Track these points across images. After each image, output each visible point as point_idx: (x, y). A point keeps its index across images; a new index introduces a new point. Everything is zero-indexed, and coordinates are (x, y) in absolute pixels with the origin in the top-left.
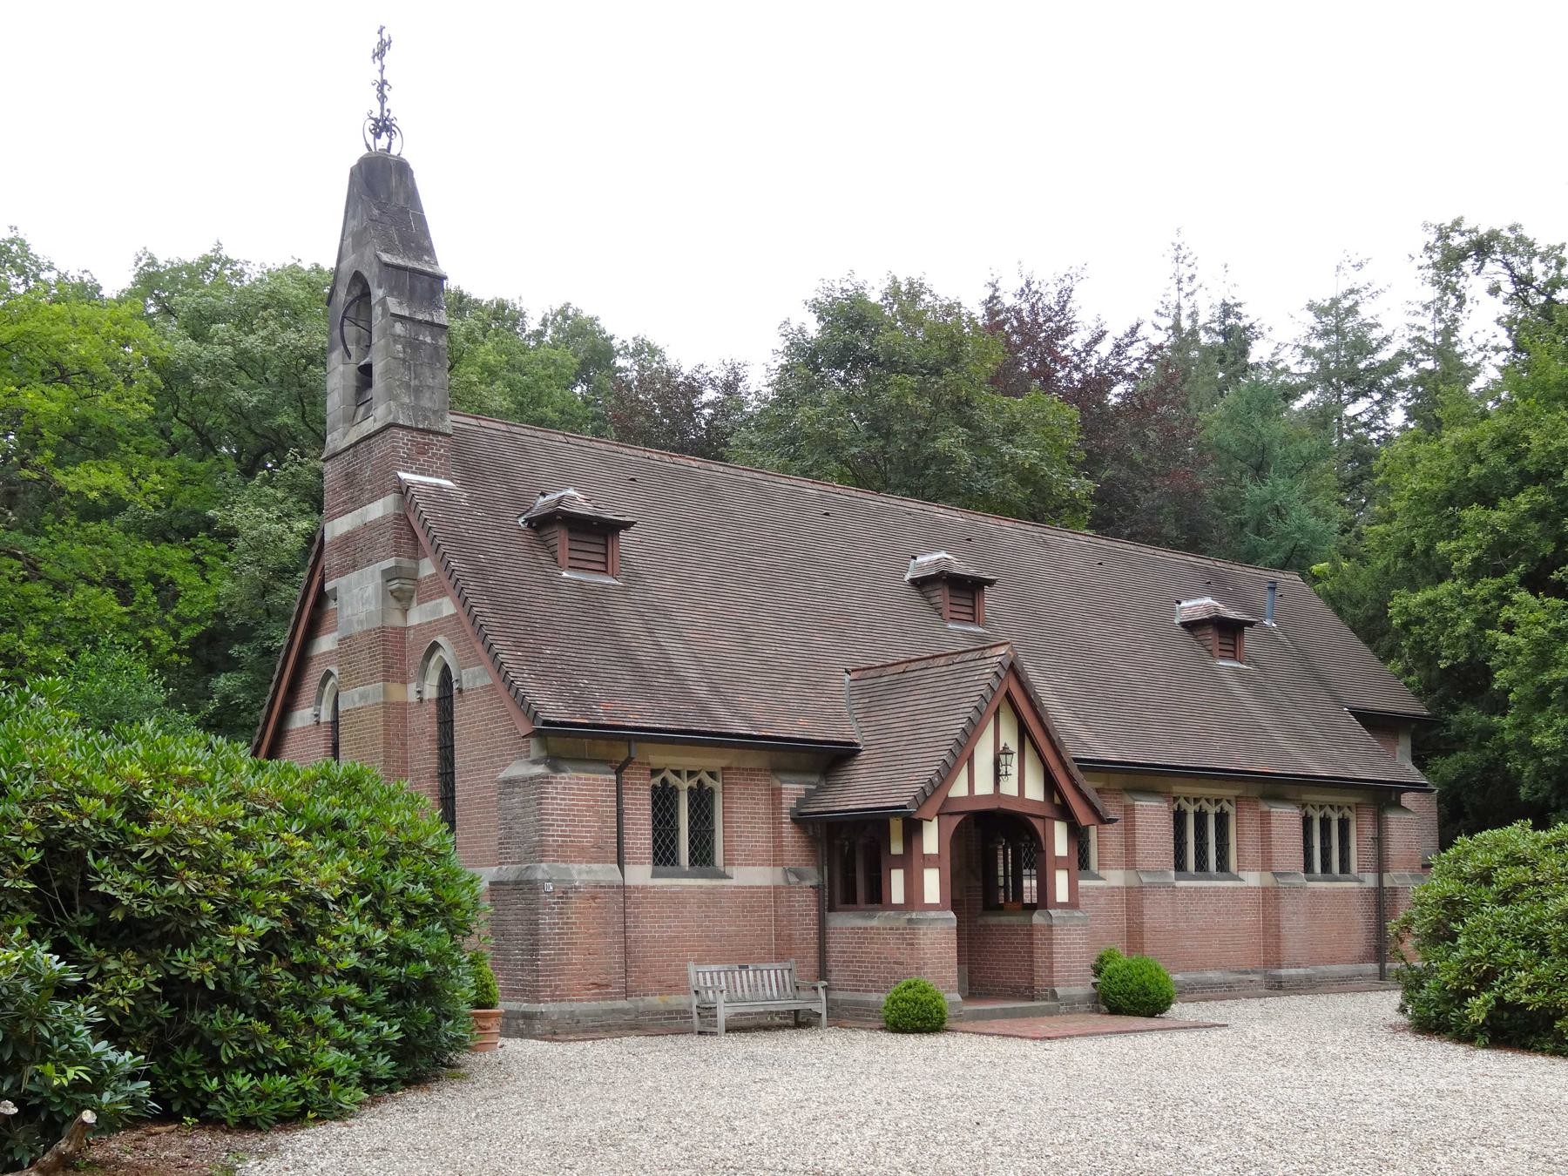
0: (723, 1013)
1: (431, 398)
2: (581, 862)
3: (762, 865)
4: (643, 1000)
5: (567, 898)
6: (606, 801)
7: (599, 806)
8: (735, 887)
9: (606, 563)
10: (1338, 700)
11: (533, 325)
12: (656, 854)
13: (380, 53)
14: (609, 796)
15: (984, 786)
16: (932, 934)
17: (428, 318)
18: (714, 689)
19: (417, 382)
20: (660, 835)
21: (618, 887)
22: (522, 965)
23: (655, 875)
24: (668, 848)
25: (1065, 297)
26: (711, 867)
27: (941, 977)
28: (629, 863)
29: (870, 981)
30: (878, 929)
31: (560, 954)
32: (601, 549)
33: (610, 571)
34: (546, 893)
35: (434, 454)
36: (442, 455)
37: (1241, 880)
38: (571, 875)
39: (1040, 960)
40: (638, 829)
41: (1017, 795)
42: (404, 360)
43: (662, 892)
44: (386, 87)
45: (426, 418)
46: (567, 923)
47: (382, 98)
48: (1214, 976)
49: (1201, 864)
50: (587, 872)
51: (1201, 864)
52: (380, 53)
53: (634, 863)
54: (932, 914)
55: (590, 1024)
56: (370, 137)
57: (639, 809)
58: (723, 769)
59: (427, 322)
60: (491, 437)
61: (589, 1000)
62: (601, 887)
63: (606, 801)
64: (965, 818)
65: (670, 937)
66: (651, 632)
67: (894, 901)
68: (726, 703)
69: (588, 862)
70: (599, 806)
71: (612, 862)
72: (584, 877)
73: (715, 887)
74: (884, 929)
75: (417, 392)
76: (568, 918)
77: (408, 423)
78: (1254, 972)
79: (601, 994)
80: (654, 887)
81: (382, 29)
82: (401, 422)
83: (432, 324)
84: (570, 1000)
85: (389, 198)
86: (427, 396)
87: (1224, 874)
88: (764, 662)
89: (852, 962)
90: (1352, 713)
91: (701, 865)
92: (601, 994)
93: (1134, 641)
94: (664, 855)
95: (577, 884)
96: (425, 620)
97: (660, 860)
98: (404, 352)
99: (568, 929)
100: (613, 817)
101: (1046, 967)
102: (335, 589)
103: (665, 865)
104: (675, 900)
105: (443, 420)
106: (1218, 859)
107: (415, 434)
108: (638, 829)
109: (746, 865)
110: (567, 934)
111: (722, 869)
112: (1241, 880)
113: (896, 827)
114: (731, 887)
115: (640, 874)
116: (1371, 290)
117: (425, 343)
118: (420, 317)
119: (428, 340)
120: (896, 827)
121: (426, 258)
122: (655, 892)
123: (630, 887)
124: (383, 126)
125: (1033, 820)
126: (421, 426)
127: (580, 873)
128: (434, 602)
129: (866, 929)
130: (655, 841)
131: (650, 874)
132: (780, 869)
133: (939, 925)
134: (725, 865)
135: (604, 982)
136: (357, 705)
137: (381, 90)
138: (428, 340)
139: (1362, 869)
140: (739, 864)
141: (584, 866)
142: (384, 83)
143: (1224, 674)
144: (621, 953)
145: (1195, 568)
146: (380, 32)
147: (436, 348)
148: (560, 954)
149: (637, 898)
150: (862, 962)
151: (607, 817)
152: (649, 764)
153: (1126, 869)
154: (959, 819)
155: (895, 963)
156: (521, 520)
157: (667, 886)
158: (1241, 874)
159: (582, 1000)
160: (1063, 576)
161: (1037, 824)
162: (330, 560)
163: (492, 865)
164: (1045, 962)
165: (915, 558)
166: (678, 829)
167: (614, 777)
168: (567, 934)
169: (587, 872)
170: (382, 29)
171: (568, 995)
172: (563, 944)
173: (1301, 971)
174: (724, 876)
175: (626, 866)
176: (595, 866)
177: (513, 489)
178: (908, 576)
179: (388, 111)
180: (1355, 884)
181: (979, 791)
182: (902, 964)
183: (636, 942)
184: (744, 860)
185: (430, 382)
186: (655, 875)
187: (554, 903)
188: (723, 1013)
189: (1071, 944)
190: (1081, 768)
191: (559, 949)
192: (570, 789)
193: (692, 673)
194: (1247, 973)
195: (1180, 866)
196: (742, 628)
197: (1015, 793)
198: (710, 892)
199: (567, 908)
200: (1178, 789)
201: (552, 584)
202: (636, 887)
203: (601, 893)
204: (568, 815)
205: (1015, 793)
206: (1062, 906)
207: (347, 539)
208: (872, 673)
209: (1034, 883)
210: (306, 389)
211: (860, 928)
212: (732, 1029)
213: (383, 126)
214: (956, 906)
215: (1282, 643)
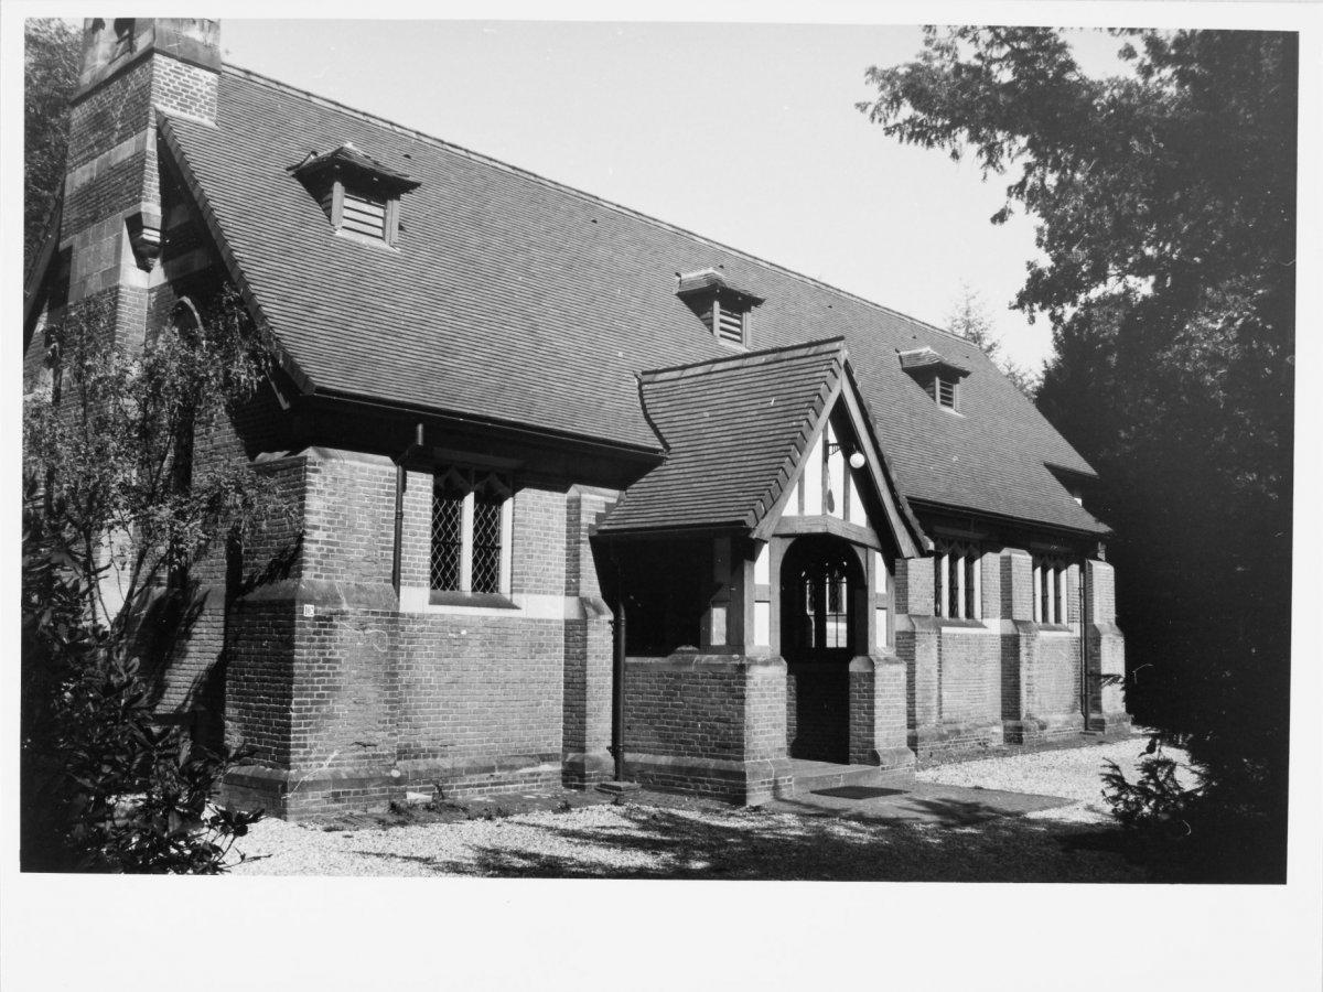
0: (198, 26)
8: (523, 620)
12: (434, 574)
22: (268, 716)
23: (434, 601)
24: (448, 567)
29: (682, 742)
39: (857, 715)
40: (417, 541)
41: (842, 518)
46: (328, 661)
53: (411, 584)
64: (794, 542)
73: (501, 620)
76: (330, 654)
91: (484, 591)
94: (443, 576)
99: (330, 668)
101: (865, 724)
103: (444, 589)
108: (417, 541)
109: (536, 592)
110: (328, 675)
111: (508, 597)
115: (415, 598)
123: (403, 615)
132: (575, 599)
134: (512, 592)
139: (1071, 620)
140: (530, 592)
150: (672, 718)
154: (789, 542)
155: (718, 720)
158: (985, 622)
161: (860, 553)
162: (71, 215)
164: (864, 719)
168: (328, 675)
174: (510, 606)
180: (1066, 634)
181: (808, 512)
182: (727, 721)
183: (408, 687)
184: (535, 586)
186: (434, 601)
187: (314, 633)
188: (198, 26)
190: (910, 504)
199: (330, 640)
202: (412, 617)
207: (89, 188)
209: (843, 626)
211: (670, 675)
212: (194, 22)
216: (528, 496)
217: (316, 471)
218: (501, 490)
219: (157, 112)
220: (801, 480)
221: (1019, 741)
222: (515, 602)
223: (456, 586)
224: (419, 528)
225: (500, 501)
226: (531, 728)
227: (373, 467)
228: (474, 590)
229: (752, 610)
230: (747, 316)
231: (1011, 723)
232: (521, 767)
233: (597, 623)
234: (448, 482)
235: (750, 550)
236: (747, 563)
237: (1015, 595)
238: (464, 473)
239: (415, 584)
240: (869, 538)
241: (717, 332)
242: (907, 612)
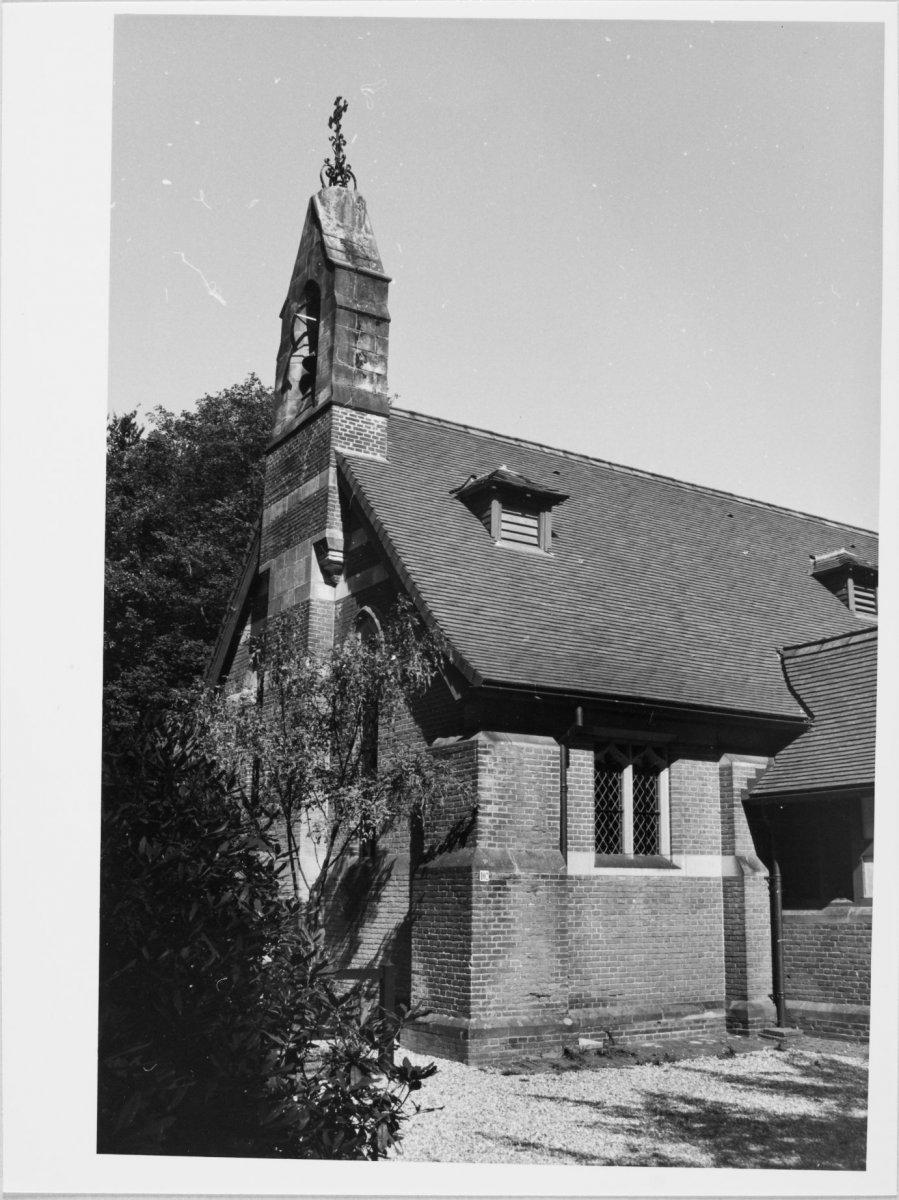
3: (711, 853)
4: (632, 1040)
5: (505, 889)
9: (538, 537)
12: (598, 840)
13: (336, 118)
14: (552, 770)
20: (602, 818)
22: (449, 970)
23: (599, 864)
26: (656, 855)
28: (571, 850)
31: (495, 958)
43: (609, 882)
46: (503, 920)
47: (339, 149)
52: (336, 118)
57: (583, 788)
73: (662, 879)
74: (858, 928)
76: (505, 914)
80: (597, 877)
81: (339, 99)
89: (817, 966)
91: (645, 853)
94: (607, 841)
100: (556, 794)
102: (268, 570)
103: (608, 853)
104: (620, 894)
107: (354, 413)
110: (503, 933)
111: (668, 858)
114: (679, 878)
115: (582, 862)
123: (571, 877)
124: (339, 173)
130: (598, 825)
131: (593, 861)
134: (672, 853)
140: (689, 853)
148: (495, 958)
149: (579, 891)
151: (550, 794)
153: (724, 854)
166: (622, 812)
170: (339, 99)
172: (500, 945)
174: (670, 866)
175: (569, 853)
179: (344, 157)
186: (599, 864)
191: (495, 952)
198: (658, 884)
202: (579, 878)
207: (280, 522)
210: (301, 1036)
213: (339, 173)
222: (675, 862)
223: (619, 850)
224: (583, 799)
226: (694, 978)
228: (636, 853)
232: (686, 1015)
233: (754, 879)
242: (734, 854)
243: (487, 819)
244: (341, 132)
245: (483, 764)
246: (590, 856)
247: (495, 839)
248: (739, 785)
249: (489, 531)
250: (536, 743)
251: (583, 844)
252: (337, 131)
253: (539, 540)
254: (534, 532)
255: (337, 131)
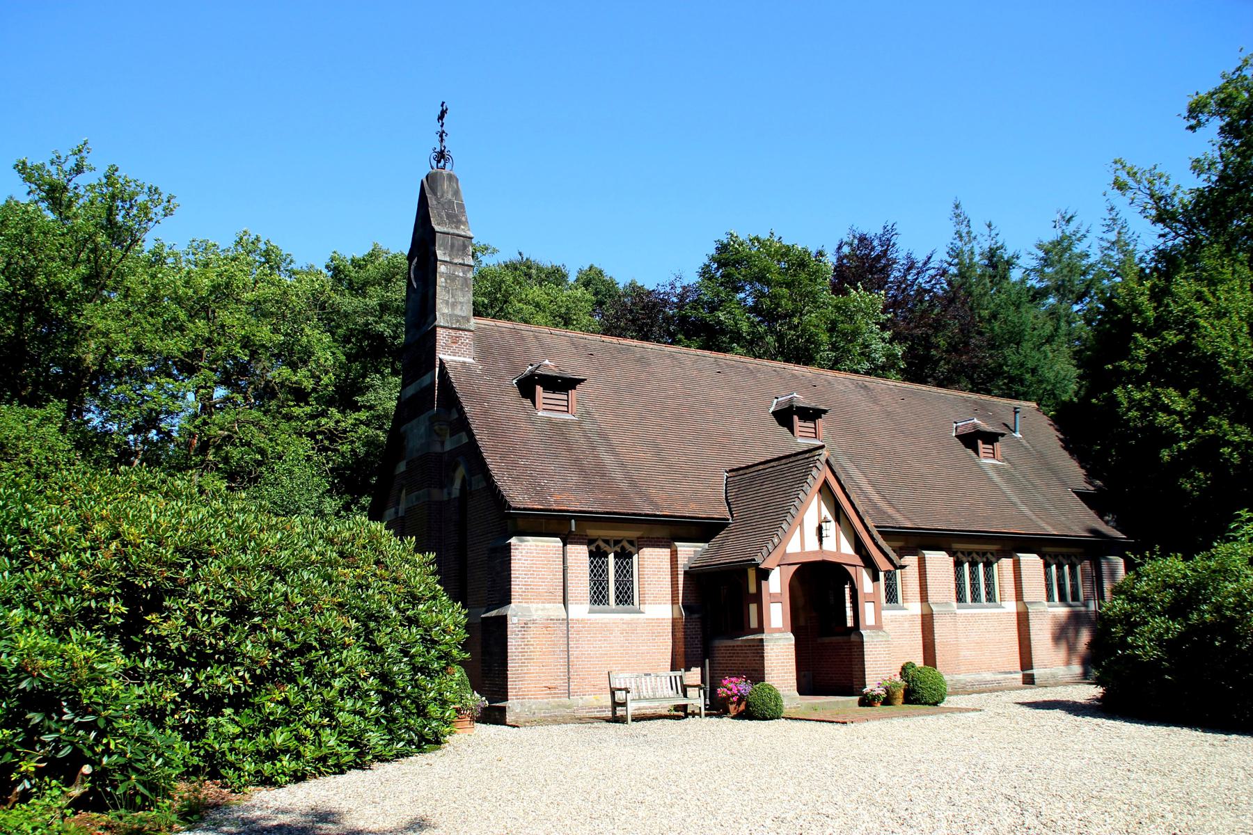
1: (461, 309)
2: (538, 603)
4: (582, 698)
6: (555, 561)
7: (551, 565)
8: (647, 619)
10: (1064, 484)
11: (621, 286)
13: (441, 117)
14: (557, 558)
15: (812, 544)
16: (777, 649)
17: (461, 261)
18: (633, 484)
19: (453, 300)
21: (563, 620)
25: (887, 244)
27: (784, 680)
30: (741, 646)
32: (813, 425)
33: (570, 411)
34: (513, 624)
35: (462, 343)
36: (467, 344)
37: (1003, 608)
38: (530, 611)
42: (446, 287)
44: (444, 135)
45: (458, 321)
46: (527, 645)
48: (988, 676)
49: (976, 598)
50: (542, 610)
51: (976, 598)
52: (441, 117)
54: (777, 635)
55: (543, 715)
56: (434, 163)
58: (638, 538)
59: (460, 264)
60: (501, 332)
61: (543, 698)
62: (551, 620)
63: (555, 561)
65: (601, 654)
66: (594, 448)
67: (773, 626)
68: (640, 493)
69: (543, 603)
70: (551, 565)
71: (559, 603)
72: (540, 612)
73: (632, 620)
75: (454, 305)
77: (446, 325)
78: (1015, 672)
79: (551, 694)
81: (443, 103)
82: (442, 324)
83: (463, 265)
84: (529, 698)
85: (442, 196)
86: (459, 307)
87: (991, 604)
88: (669, 466)
90: (1074, 492)
92: (551, 694)
93: (926, 448)
94: (598, 596)
95: (535, 618)
96: (453, 447)
97: (621, 601)
98: (446, 282)
105: (469, 322)
106: (988, 593)
110: (527, 652)
112: (1003, 608)
113: (752, 574)
115: (580, 609)
116: (1078, 235)
117: (459, 276)
118: (456, 261)
119: (461, 274)
120: (752, 574)
121: (462, 227)
122: (591, 624)
124: (441, 156)
125: (848, 568)
126: (454, 326)
127: (536, 610)
128: (457, 436)
129: (734, 646)
131: (588, 610)
133: (781, 643)
135: (553, 685)
136: (415, 504)
137: (441, 136)
138: (461, 274)
141: (540, 606)
142: (443, 132)
143: (986, 468)
144: (565, 665)
145: (966, 401)
146: (442, 105)
147: (466, 279)
152: (586, 536)
155: (752, 670)
156: (515, 381)
157: (599, 619)
159: (537, 698)
160: (877, 409)
163: (482, 607)
165: (777, 398)
167: (561, 544)
168: (527, 652)
169: (542, 610)
170: (443, 103)
171: (527, 695)
173: (1048, 671)
174: (640, 612)
176: (547, 606)
177: (512, 363)
178: (772, 410)
179: (445, 147)
181: (807, 549)
182: (756, 670)
183: (577, 658)
185: (461, 299)
186: (591, 612)
189: (878, 654)
190: (880, 532)
192: (531, 553)
193: (618, 475)
194: (1010, 673)
195: (960, 598)
196: (656, 445)
197: (834, 549)
200: (956, 546)
201: (531, 420)
203: (550, 623)
204: (530, 571)
205: (834, 549)
206: (870, 628)
208: (741, 472)
213: (441, 156)
214: (795, 629)
215: (1026, 449)
216: (647, 552)
217: (517, 549)
218: (993, 559)
219: (440, 359)
220: (801, 524)
221: (1033, 683)
224: (580, 573)
225: (630, 556)
227: (543, 544)
229: (769, 608)
230: (819, 421)
231: (1029, 672)
234: (958, 558)
235: (764, 574)
236: (763, 582)
237: (918, 589)
238: (607, 542)
239: (578, 602)
240: (857, 560)
241: (981, 454)
243: (517, 587)
244: (444, 128)
245: (434, 574)
246: (587, 606)
247: (522, 599)
248: (683, 562)
249: (535, 406)
250: (542, 541)
251: (580, 600)
252: (442, 126)
253: (815, 433)
254: (991, 451)
255: (442, 126)
